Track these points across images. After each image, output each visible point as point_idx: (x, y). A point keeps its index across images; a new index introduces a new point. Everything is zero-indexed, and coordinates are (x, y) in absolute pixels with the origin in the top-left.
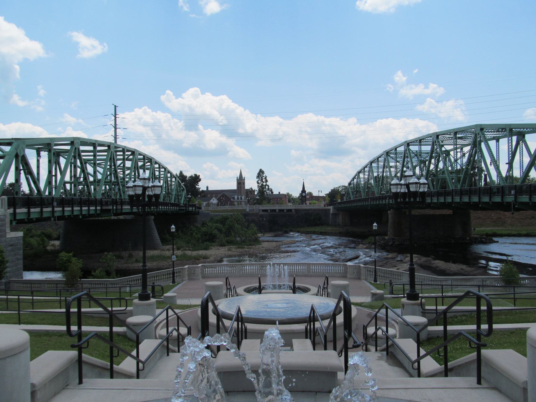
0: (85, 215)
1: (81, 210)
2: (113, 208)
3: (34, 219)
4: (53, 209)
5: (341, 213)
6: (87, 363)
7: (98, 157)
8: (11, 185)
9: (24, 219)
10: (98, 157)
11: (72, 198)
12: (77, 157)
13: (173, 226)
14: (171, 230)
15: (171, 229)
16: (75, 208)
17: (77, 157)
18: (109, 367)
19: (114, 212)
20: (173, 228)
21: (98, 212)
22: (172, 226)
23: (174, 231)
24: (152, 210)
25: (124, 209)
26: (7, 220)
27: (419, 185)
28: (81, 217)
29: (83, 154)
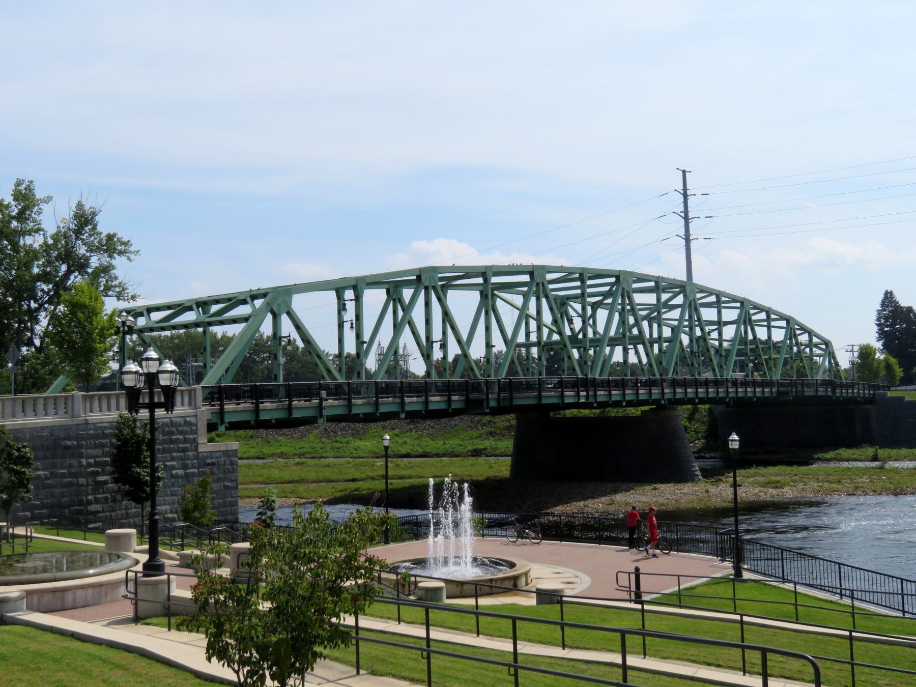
0: (760, 397)
1: (697, 392)
2: (792, 390)
3: (273, 421)
4: (321, 403)
5: (252, 547)
6: (800, 593)
7: (589, 290)
8: (456, 359)
9: (249, 422)
10: (589, 290)
11: (401, 381)
12: (542, 294)
13: (735, 437)
14: (728, 444)
15: (730, 443)
16: (749, 390)
17: (542, 294)
18: (851, 605)
19: (794, 394)
20: (732, 440)
21: (774, 395)
22: (731, 435)
23: (737, 447)
24: (838, 395)
25: (431, 401)
26: (199, 425)
27: (780, 551)
28: (755, 400)
29: (551, 286)
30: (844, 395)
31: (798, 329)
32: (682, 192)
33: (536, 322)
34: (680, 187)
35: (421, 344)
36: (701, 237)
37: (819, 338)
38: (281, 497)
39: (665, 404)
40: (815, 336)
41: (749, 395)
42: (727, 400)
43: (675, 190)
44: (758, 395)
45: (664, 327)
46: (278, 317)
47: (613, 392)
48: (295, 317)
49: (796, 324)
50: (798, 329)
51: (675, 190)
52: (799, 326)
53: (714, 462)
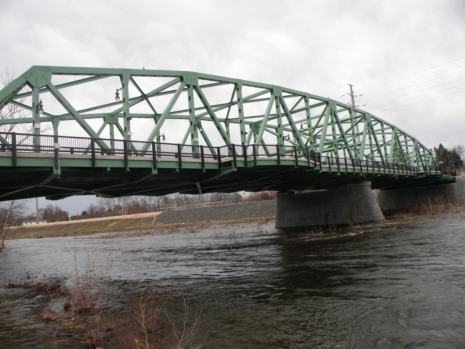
30: (409, 174)
31: (373, 121)
32: (351, 94)
33: (212, 122)
34: (350, 92)
35: (122, 130)
36: (361, 105)
37: (387, 125)
38: (38, 238)
39: (363, 176)
40: (385, 124)
41: (376, 172)
42: (395, 176)
43: (348, 94)
44: (342, 171)
45: (204, 106)
46: (117, 124)
47: (438, 171)
48: (249, 138)
49: (372, 117)
50: (373, 121)
51: (348, 94)
52: (373, 118)
53: (333, 258)
